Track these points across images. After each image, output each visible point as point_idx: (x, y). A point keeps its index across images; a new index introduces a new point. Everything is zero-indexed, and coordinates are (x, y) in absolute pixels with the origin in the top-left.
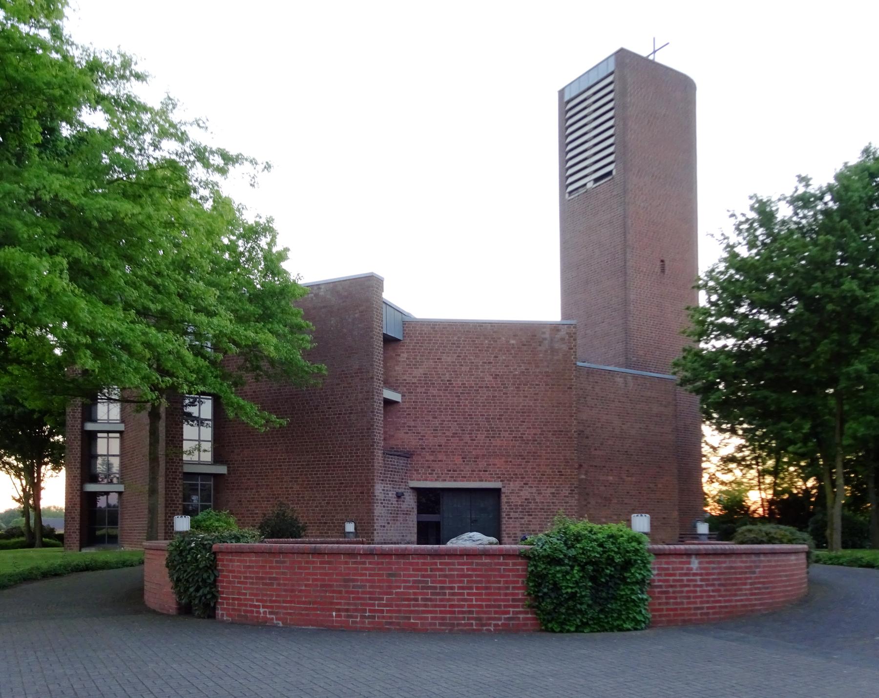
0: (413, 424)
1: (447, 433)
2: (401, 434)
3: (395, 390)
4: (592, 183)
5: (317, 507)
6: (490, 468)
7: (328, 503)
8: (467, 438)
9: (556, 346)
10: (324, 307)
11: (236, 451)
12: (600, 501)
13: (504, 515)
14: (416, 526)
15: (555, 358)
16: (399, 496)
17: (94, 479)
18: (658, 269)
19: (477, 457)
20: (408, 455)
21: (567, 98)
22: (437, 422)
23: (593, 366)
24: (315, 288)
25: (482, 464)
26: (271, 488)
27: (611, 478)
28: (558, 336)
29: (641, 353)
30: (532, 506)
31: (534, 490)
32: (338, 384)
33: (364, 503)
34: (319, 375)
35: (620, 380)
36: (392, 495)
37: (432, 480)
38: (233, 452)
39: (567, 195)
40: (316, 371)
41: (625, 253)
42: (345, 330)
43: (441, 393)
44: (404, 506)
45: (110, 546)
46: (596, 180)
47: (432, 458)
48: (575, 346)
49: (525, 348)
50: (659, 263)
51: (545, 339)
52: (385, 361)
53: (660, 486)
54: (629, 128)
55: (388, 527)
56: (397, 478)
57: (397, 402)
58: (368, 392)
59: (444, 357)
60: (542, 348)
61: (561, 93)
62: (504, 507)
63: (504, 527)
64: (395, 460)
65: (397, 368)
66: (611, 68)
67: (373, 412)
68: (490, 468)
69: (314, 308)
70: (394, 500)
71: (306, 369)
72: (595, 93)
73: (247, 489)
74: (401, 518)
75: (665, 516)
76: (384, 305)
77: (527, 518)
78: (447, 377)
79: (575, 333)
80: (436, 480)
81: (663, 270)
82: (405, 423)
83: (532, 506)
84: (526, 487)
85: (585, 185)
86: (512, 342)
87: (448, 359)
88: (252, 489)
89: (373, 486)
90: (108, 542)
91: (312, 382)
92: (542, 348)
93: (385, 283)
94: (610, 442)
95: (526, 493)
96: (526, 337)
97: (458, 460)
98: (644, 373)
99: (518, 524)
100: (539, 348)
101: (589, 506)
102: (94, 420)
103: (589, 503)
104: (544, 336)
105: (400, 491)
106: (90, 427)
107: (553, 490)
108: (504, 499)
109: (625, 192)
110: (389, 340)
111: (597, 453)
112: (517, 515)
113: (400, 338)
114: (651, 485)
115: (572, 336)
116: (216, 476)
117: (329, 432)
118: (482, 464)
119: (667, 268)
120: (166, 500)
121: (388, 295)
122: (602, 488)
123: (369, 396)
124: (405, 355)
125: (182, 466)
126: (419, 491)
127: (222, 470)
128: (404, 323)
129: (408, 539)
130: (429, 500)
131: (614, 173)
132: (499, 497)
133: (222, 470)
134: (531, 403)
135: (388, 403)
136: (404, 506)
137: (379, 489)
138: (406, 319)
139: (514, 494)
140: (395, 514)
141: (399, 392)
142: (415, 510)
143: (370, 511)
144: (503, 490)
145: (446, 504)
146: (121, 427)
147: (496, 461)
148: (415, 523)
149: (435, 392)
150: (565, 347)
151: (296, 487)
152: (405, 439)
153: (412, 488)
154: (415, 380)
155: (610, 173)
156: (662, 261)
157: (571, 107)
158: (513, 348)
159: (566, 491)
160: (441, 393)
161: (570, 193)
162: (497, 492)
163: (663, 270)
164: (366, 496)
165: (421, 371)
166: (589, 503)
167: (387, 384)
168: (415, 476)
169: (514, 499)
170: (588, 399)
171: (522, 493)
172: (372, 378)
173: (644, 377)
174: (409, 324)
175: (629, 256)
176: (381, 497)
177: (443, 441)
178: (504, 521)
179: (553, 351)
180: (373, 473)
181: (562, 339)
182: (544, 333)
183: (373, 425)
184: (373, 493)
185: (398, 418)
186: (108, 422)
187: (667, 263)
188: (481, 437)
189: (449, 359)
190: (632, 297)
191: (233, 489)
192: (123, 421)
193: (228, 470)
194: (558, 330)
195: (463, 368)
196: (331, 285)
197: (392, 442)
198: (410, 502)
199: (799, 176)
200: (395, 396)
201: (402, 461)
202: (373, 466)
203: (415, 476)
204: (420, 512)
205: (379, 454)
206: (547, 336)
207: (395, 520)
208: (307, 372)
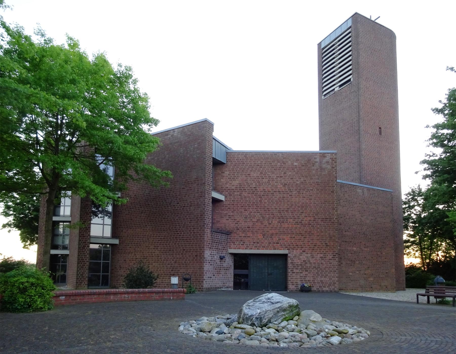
0: (232, 214)
1: (254, 220)
2: (224, 220)
3: (221, 193)
4: (338, 87)
5: (168, 264)
6: (281, 241)
7: (175, 262)
8: (266, 223)
9: (324, 166)
10: (176, 142)
11: (124, 230)
12: (348, 262)
13: (289, 270)
14: (233, 277)
15: (323, 173)
16: (222, 258)
17: (55, 247)
18: (378, 132)
19: (272, 234)
20: (228, 233)
21: (322, 47)
22: (247, 213)
23: (343, 182)
24: (172, 132)
25: (275, 239)
26: (143, 253)
27: (355, 249)
28: (325, 160)
29: (369, 178)
30: (308, 265)
31: (309, 255)
32: (184, 188)
33: (198, 262)
34: (167, 179)
35: (359, 191)
36: (217, 257)
37: (243, 249)
38: (122, 231)
39: (323, 97)
40: (164, 175)
41: (359, 122)
42: (188, 155)
43: (250, 195)
44: (225, 265)
45: (61, 284)
46: (340, 86)
47: (243, 235)
48: (336, 166)
49: (303, 168)
50: (378, 129)
51: (316, 162)
52: (214, 177)
53: (384, 253)
54: (358, 62)
55: (213, 278)
56: (220, 247)
57: (222, 201)
58: (202, 192)
59: (252, 173)
60: (315, 168)
61: (319, 45)
62: (290, 265)
63: (289, 278)
64: (219, 236)
65: (222, 180)
66: (350, 24)
67: (204, 205)
68: (281, 241)
69: (171, 144)
70: (218, 261)
71: (157, 174)
72: (334, 58)
73: (129, 253)
74: (223, 272)
75: (387, 271)
76: (214, 141)
77: (304, 273)
78: (254, 185)
79: (335, 158)
80: (246, 249)
81: (380, 133)
82: (227, 214)
83: (308, 265)
84: (304, 254)
85: (334, 89)
86: (295, 164)
87: (254, 175)
88: (132, 253)
89: (203, 252)
90: (61, 282)
91: (164, 183)
92: (315, 168)
93: (214, 126)
94: (354, 227)
95: (304, 257)
96: (305, 158)
97: (260, 237)
98: (374, 188)
99: (298, 277)
100: (313, 168)
101: (342, 265)
102: (59, 216)
103: (342, 263)
104: (316, 160)
105: (222, 255)
106: (55, 219)
107: (322, 255)
108: (289, 261)
109: (359, 89)
110: (217, 163)
111: (347, 233)
112: (298, 271)
113: (224, 161)
114: (379, 253)
115: (334, 160)
116: (112, 245)
117: (177, 218)
118: (275, 239)
119: (382, 132)
120: (78, 259)
121: (216, 134)
122: (350, 255)
123: (202, 195)
124: (228, 173)
125: (89, 239)
126: (234, 255)
127: (116, 242)
128: (227, 153)
129: (227, 285)
130: (241, 261)
131: (352, 80)
132: (286, 260)
133: (116, 242)
134: (307, 201)
135: (215, 201)
136: (225, 265)
137: (207, 254)
138: (229, 151)
139: (296, 257)
140: (218, 270)
141: (223, 195)
142: (233, 267)
143: (201, 268)
144: (289, 255)
145: (252, 263)
146: (69, 219)
147: (285, 237)
148: (233, 275)
149: (246, 195)
150: (329, 167)
151: (157, 252)
152: (226, 223)
153: (231, 254)
154: (234, 188)
155: (350, 80)
156: (380, 128)
157: (325, 53)
158: (296, 168)
159: (330, 256)
160: (250, 195)
161: (325, 95)
162: (285, 256)
163: (380, 133)
164: (199, 258)
165: (237, 182)
166: (342, 263)
167: (215, 189)
168: (232, 246)
169: (296, 261)
170: (341, 201)
171: (301, 257)
172: (204, 183)
173: (374, 190)
174: (229, 154)
175: (361, 124)
176: (209, 258)
177: (251, 224)
178: (289, 274)
179: (321, 169)
180: (204, 243)
181: (328, 162)
182: (315, 158)
183: (204, 213)
184: (203, 256)
185: (223, 210)
186: (64, 216)
187: (382, 129)
188: (275, 222)
189: (255, 175)
190: (363, 147)
191: (121, 253)
192: (71, 216)
193: (119, 242)
194: (325, 157)
195: (264, 180)
196: (181, 129)
197: (218, 225)
198: (229, 262)
199: (432, 109)
200: (221, 197)
201: (224, 237)
202: (204, 239)
203: (232, 246)
204: (235, 268)
205: (208, 232)
206: (318, 160)
207: (219, 273)
208: (158, 177)
